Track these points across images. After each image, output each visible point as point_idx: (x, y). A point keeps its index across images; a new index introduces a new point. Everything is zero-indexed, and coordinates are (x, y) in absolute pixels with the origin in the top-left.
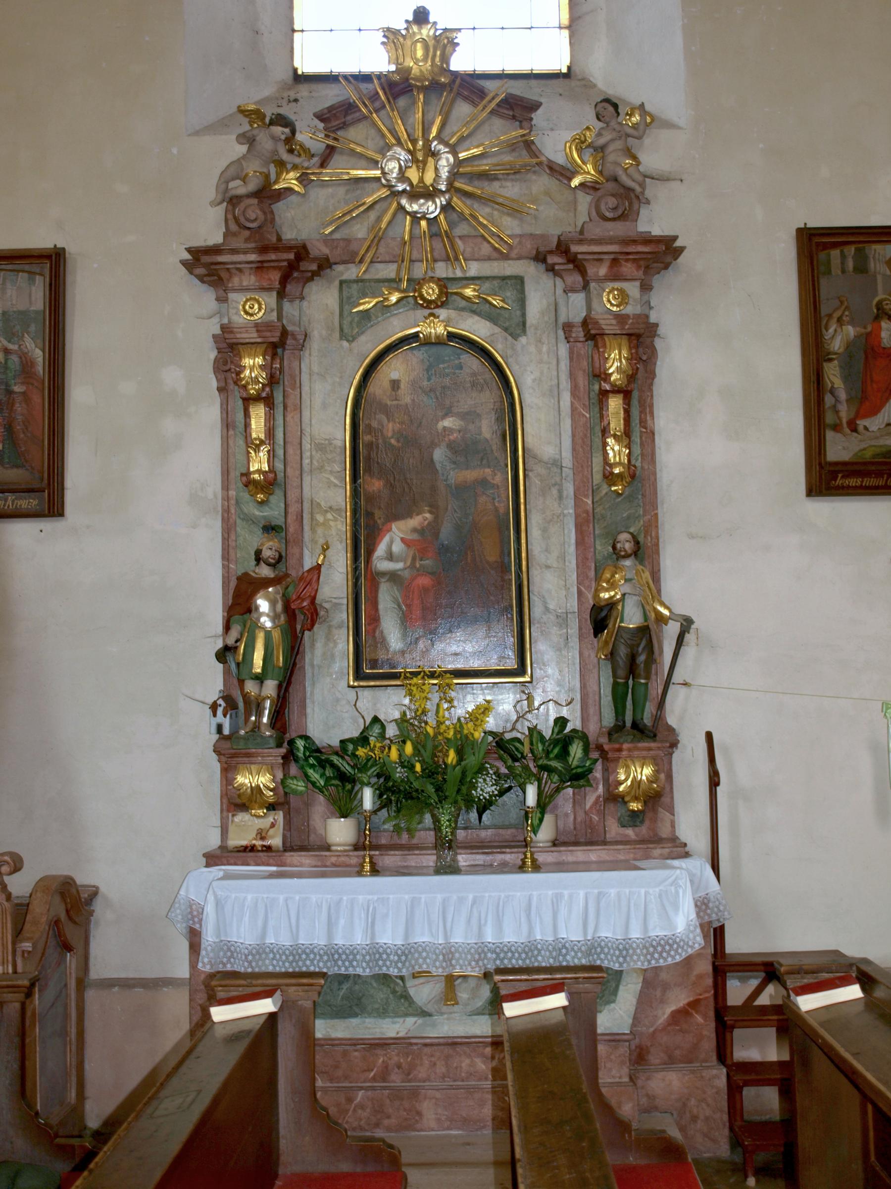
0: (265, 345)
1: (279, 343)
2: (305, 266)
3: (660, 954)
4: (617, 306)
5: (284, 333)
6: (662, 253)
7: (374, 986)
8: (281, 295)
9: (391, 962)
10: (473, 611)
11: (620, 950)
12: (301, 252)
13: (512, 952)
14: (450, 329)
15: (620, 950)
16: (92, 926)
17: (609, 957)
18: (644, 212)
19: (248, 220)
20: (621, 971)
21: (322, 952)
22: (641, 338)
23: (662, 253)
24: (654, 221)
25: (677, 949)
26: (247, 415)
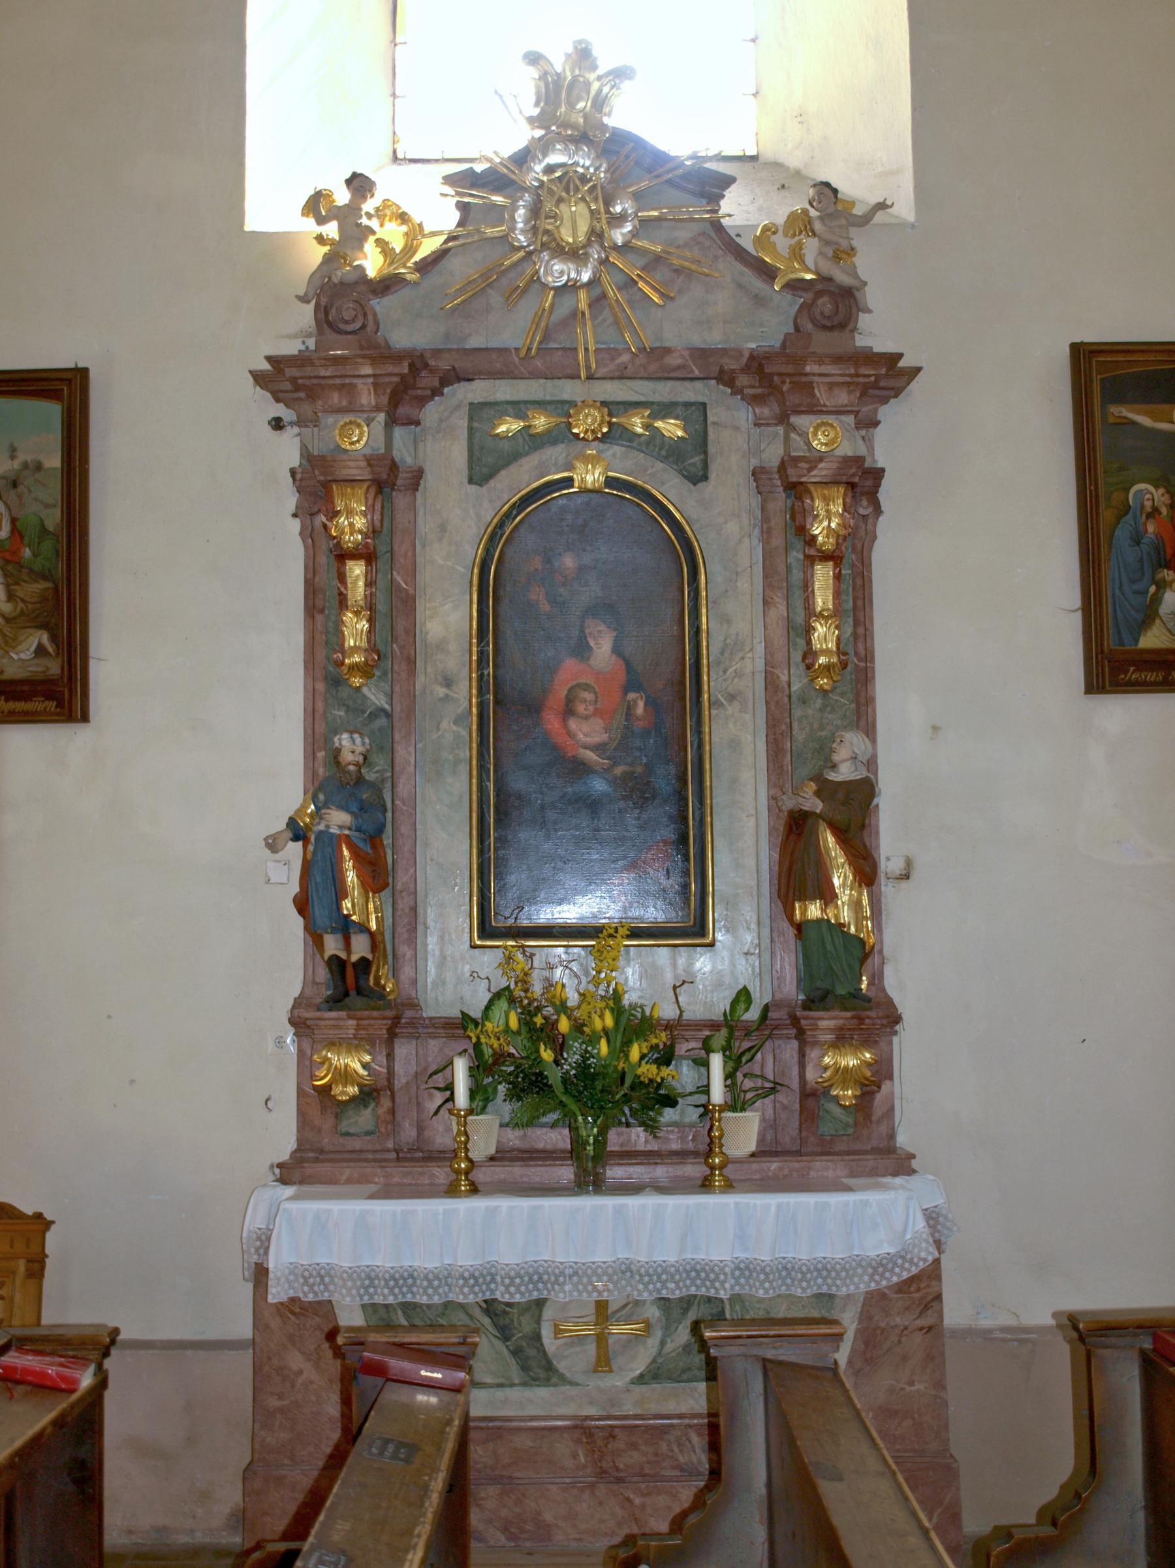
0: (365, 485)
1: (389, 481)
2: (427, 380)
3: (704, 1280)
4: (826, 444)
5: (394, 467)
6: (885, 377)
7: (510, 1322)
8: (392, 421)
9: (793, 1280)
10: (570, 883)
11: (802, 1273)
12: (417, 362)
13: (827, 1270)
14: (610, 474)
15: (802, 1273)
16: (884, 917)
17: (549, 1286)
18: (864, 320)
19: (347, 322)
20: (545, 1300)
21: (387, 1276)
22: (862, 483)
23: (885, 377)
24: (876, 332)
25: (883, 1273)
26: (342, 577)
